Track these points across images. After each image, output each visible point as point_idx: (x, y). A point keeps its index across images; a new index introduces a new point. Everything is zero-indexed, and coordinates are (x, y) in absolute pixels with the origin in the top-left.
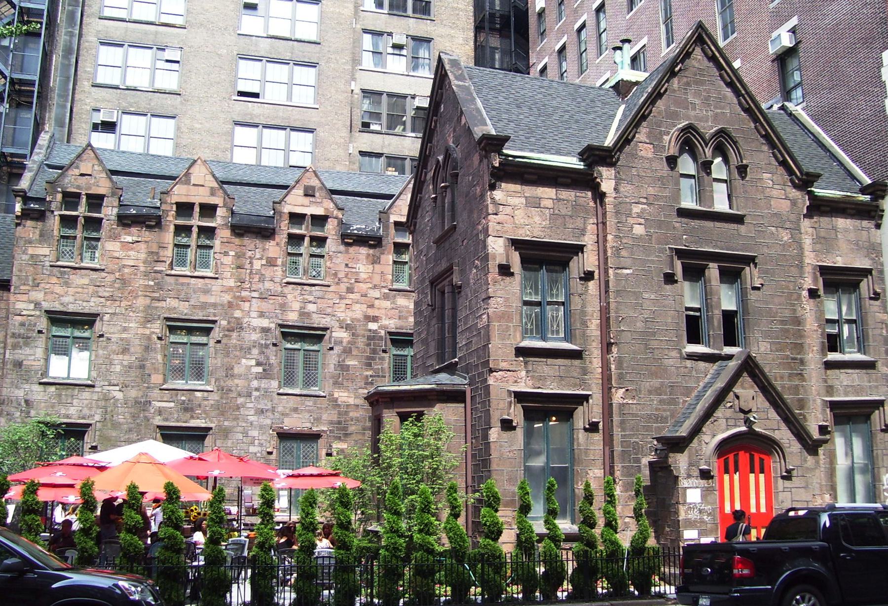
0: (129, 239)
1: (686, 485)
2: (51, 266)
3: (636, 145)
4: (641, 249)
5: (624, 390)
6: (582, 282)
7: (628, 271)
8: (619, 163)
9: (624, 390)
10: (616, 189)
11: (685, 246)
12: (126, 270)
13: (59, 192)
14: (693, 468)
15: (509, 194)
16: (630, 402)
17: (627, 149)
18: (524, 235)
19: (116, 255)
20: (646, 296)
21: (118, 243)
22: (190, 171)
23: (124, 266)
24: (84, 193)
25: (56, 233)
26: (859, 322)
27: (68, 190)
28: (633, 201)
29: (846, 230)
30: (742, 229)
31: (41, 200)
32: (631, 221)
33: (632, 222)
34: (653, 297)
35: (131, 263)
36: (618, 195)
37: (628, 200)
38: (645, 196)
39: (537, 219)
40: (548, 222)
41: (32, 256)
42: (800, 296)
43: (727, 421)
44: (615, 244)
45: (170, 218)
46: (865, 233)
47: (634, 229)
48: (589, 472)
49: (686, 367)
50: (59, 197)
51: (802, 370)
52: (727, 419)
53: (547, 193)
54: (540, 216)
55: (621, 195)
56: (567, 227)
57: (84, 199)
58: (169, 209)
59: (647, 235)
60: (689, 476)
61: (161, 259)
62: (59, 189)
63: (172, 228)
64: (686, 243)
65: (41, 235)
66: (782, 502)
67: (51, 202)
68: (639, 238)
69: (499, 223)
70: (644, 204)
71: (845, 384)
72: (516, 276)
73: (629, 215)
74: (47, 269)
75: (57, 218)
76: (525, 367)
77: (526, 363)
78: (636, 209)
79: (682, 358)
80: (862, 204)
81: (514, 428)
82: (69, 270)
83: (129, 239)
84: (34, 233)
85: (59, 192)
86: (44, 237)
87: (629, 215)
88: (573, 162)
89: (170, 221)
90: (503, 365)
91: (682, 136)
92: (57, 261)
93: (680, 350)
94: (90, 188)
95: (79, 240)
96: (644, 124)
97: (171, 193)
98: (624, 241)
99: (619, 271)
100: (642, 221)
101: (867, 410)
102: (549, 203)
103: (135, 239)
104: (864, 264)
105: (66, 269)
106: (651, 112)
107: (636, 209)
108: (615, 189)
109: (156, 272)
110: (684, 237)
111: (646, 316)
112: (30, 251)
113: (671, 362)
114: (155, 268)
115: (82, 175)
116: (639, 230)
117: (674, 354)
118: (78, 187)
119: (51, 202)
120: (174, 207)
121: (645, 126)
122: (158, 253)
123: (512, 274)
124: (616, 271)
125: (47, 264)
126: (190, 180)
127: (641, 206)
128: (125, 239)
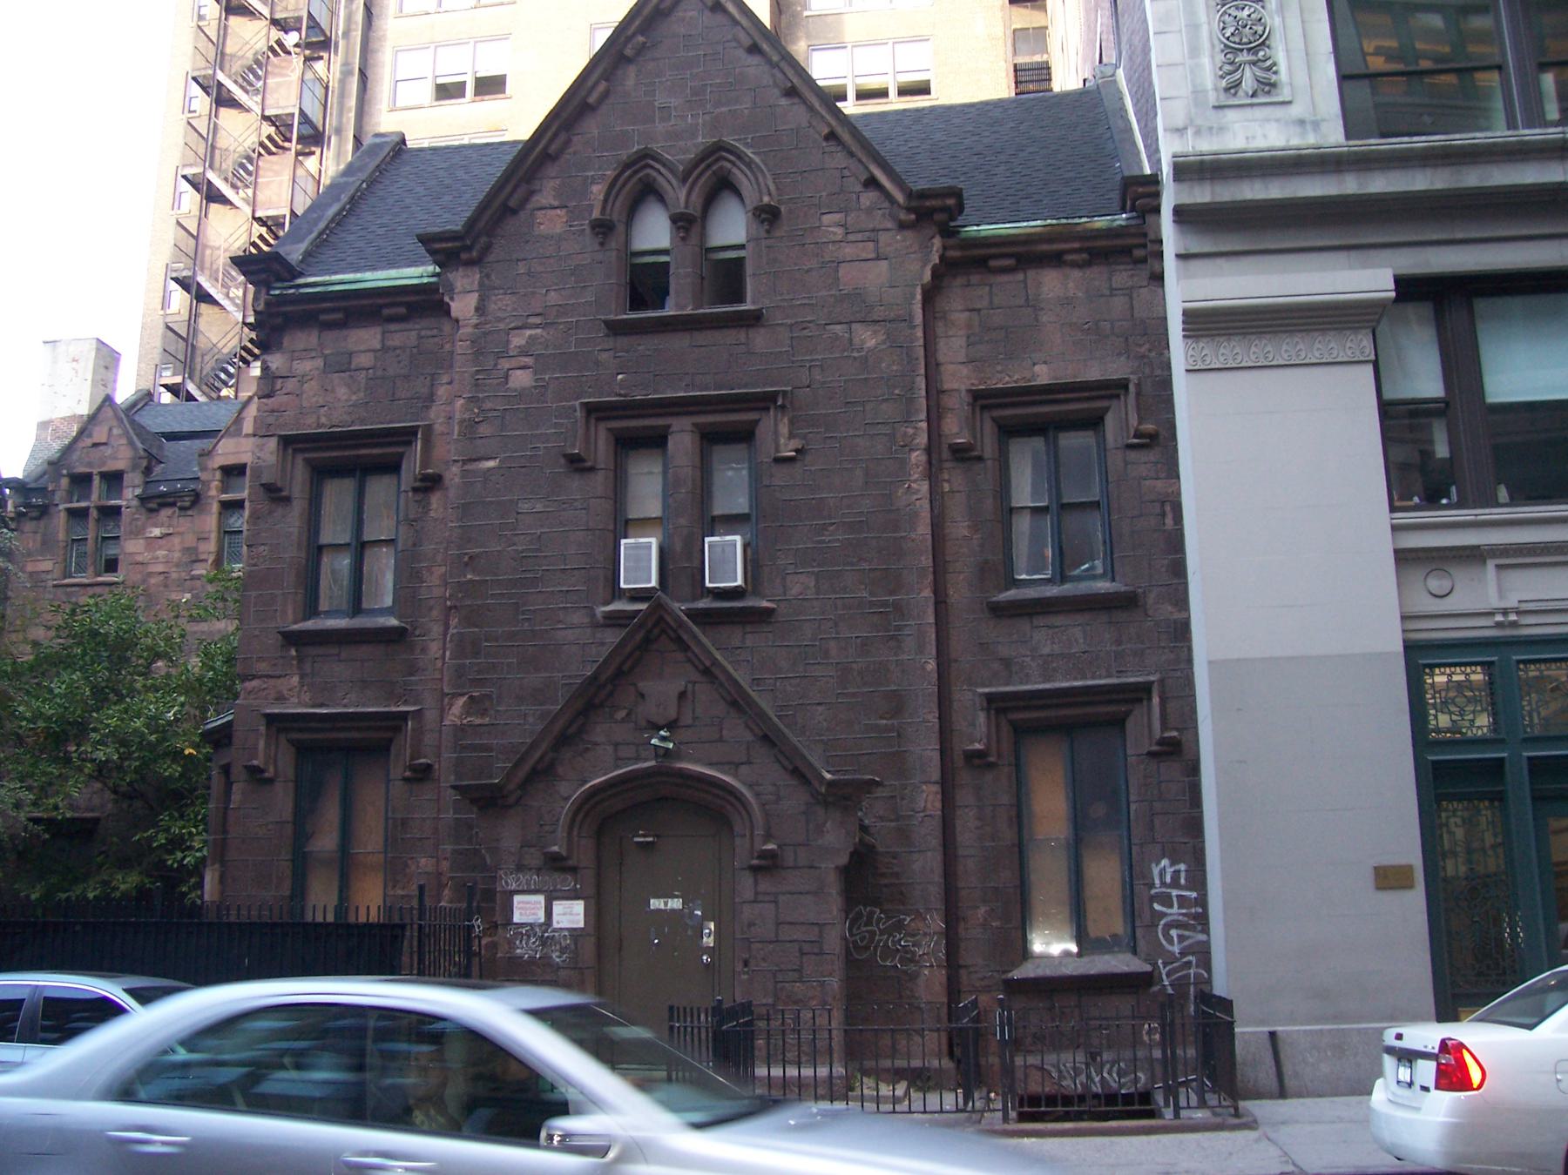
0: (157, 532)
1: (514, 887)
2: (55, 586)
3: (532, 215)
4: (522, 416)
5: (465, 698)
6: (417, 498)
7: (491, 464)
8: (491, 258)
9: (465, 698)
10: (480, 310)
11: (620, 395)
12: (153, 581)
13: (64, 476)
14: (532, 850)
15: (294, 356)
16: (478, 721)
17: (511, 225)
18: (315, 425)
19: (139, 558)
20: (525, 507)
21: (141, 541)
22: (242, 416)
23: (150, 574)
24: (95, 471)
25: (61, 536)
26: (1104, 504)
27: (75, 471)
28: (512, 325)
29: (1067, 302)
30: (760, 339)
31: (42, 491)
32: (505, 364)
33: (507, 366)
34: (539, 507)
35: (160, 568)
36: (483, 319)
37: (502, 326)
38: (539, 311)
39: (342, 392)
40: (362, 394)
41: (31, 574)
42: (903, 463)
43: (616, 750)
44: (466, 416)
45: (213, 492)
46: (1119, 302)
47: (511, 379)
48: (409, 862)
49: (603, 644)
50: (65, 482)
51: (899, 628)
52: (616, 745)
53: (364, 340)
54: (348, 386)
55: (490, 318)
56: (397, 397)
57: (96, 480)
58: (210, 478)
59: (535, 387)
60: (520, 868)
61: (202, 557)
62: (65, 472)
63: (215, 507)
64: (620, 385)
65: (44, 543)
66: (751, 924)
67: (53, 492)
68: (521, 394)
69: (273, 411)
70: (537, 326)
71: (1046, 651)
72: (295, 503)
73: (503, 354)
74: (50, 592)
75: (63, 515)
76: (300, 668)
77: (300, 659)
78: (518, 340)
79: (595, 625)
80: (1110, 233)
81: (271, 781)
82: (77, 589)
83: (157, 532)
84: (34, 541)
85: (64, 476)
86: (47, 544)
87: (503, 354)
88: (417, 273)
89: (213, 497)
90: (263, 667)
91: (630, 177)
92: (65, 578)
93: (592, 609)
94: (104, 464)
95: (90, 542)
96: (552, 170)
97: (214, 453)
98: (488, 405)
99: (469, 467)
100: (528, 361)
101: (1112, 708)
102: (364, 360)
103: (165, 531)
104: (1115, 369)
105: (73, 589)
106: (568, 143)
107: (518, 340)
108: (477, 309)
109: (193, 578)
110: (620, 377)
111: (520, 548)
112: (30, 568)
113: (570, 635)
114: (193, 573)
115: (95, 445)
116: (521, 379)
117: (578, 618)
118: (90, 464)
119: (53, 492)
120: (218, 475)
121: (553, 175)
122: (196, 549)
123: (287, 500)
124: (466, 467)
125: (50, 583)
126: (241, 429)
127: (528, 332)
128: (151, 532)
